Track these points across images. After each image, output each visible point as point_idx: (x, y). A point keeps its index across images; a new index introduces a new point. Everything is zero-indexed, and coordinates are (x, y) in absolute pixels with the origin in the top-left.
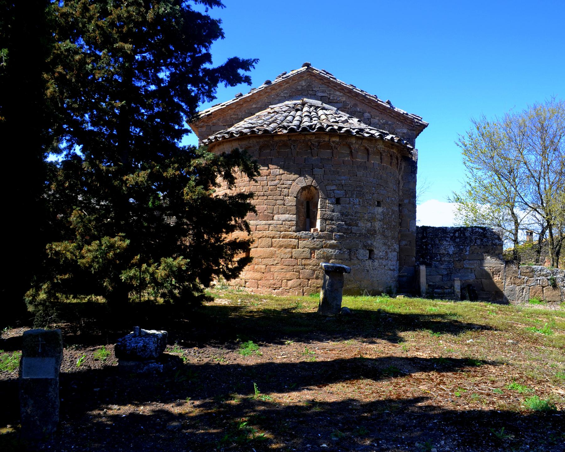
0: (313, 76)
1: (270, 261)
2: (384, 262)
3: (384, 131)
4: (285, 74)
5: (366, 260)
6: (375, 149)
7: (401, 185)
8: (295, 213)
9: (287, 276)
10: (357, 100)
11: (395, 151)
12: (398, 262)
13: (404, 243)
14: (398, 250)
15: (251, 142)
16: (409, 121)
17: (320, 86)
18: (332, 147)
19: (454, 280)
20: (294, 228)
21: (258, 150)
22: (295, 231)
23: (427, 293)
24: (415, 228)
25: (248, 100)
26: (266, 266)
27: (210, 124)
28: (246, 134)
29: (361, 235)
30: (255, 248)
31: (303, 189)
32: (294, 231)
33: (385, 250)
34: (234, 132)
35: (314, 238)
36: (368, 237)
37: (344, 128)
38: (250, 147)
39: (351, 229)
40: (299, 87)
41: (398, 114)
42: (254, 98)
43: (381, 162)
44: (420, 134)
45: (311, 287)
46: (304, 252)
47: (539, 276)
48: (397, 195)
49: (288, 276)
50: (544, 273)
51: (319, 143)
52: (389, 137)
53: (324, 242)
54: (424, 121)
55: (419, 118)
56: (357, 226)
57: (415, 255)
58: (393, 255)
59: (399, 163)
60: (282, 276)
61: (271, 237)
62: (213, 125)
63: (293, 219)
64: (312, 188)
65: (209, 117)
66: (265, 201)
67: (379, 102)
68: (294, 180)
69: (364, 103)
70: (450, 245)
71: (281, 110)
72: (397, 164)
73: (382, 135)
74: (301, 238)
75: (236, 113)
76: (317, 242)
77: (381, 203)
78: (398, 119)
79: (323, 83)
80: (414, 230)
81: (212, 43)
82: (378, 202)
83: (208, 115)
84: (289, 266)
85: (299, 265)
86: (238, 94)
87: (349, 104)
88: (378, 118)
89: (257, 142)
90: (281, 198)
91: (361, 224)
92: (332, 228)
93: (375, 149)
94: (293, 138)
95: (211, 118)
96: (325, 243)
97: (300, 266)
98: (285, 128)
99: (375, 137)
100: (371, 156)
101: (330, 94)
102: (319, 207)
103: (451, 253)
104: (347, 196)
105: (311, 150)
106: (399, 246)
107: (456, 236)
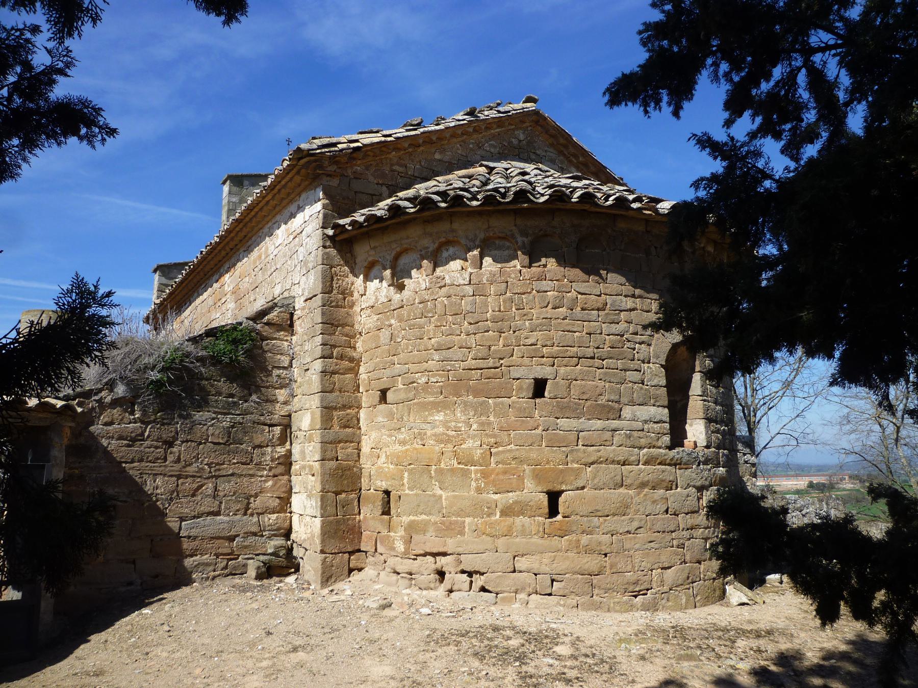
9: (663, 558)
20: (667, 439)
40: (513, 140)
45: (705, 581)
49: (665, 557)
60: (651, 559)
62: (355, 178)
74: (680, 464)
79: (552, 145)
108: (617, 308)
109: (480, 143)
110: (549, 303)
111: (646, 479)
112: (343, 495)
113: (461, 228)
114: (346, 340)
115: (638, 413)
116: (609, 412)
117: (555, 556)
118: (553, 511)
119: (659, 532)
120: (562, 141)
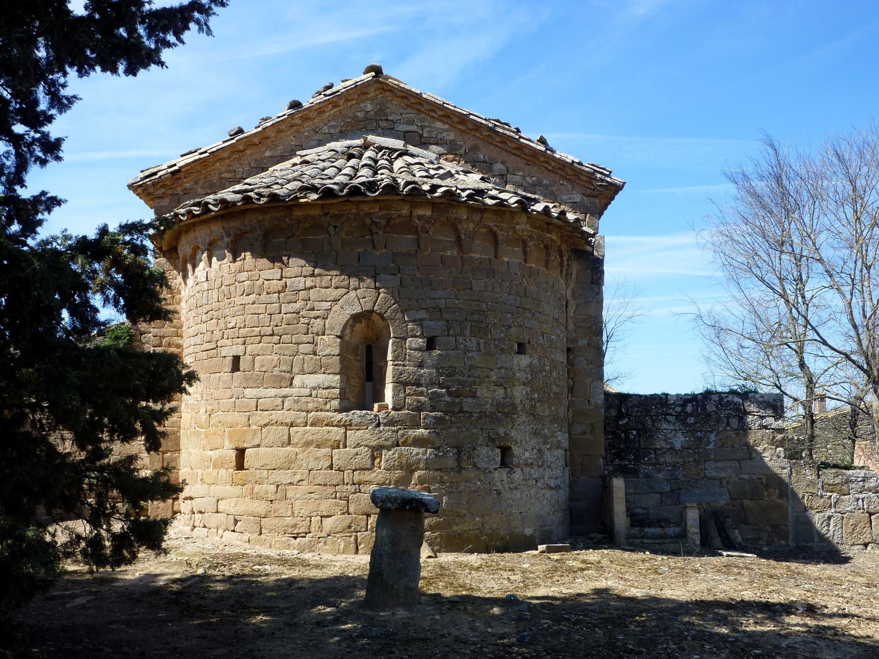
0: (388, 91)
1: (284, 477)
2: (535, 472)
3: (529, 195)
4: (330, 87)
5: (495, 469)
6: (511, 233)
7: (572, 309)
8: (338, 371)
9: (323, 508)
10: (479, 138)
11: (554, 238)
12: (568, 469)
13: (578, 429)
14: (565, 444)
15: (246, 222)
16: (585, 179)
17: (402, 111)
18: (416, 228)
19: (685, 508)
20: (335, 403)
21: (260, 238)
22: (339, 411)
23: (629, 536)
24: (602, 396)
25: (256, 141)
26: (278, 486)
27: (179, 190)
28: (234, 204)
29: (482, 415)
30: (254, 447)
31: (356, 318)
32: (335, 411)
33: (537, 447)
34: (210, 201)
35: (378, 425)
36: (499, 420)
37: (443, 186)
38: (246, 233)
39: (461, 402)
40: (359, 114)
41: (562, 164)
42: (268, 138)
43: (525, 261)
44: (609, 207)
46: (357, 454)
47: (861, 492)
48: (563, 329)
49: (325, 507)
50: (872, 485)
51: (389, 220)
52: (539, 207)
53: (401, 432)
54: (616, 178)
55: (605, 172)
56: (474, 395)
57: (603, 453)
58: (556, 457)
59: (565, 263)
61: (287, 425)
62: (185, 194)
63: (333, 385)
64: (375, 317)
65: (177, 176)
66: (275, 346)
67: (522, 140)
68: (336, 301)
69: (492, 144)
70: (676, 430)
71: (317, 158)
72: (562, 264)
73: (524, 204)
75: (231, 168)
76: (387, 432)
77: (527, 346)
78: (563, 174)
79: (408, 106)
80: (600, 402)
81: (189, 29)
82: (520, 345)
83: (173, 173)
84: (325, 485)
85: (347, 484)
86: (234, 128)
87: (461, 147)
88: (521, 173)
89: (259, 221)
90: (212, 347)
91: (483, 392)
92: (419, 401)
93: (511, 233)
94: (334, 211)
95: (180, 179)
96: (403, 435)
97: (349, 487)
98: (313, 189)
99: (509, 206)
100: (502, 248)
101: (423, 127)
102: (390, 357)
103: (678, 446)
104: (451, 332)
105: (372, 234)
106: (570, 435)
107: (686, 413)
108: (295, 289)
109: (316, 128)
110: (244, 291)
111: (311, 438)
112: (169, 454)
113: (201, 235)
114: (173, 331)
115: (307, 382)
116: (281, 381)
117: (237, 501)
118: (240, 465)
119: (319, 485)
120: (413, 100)
